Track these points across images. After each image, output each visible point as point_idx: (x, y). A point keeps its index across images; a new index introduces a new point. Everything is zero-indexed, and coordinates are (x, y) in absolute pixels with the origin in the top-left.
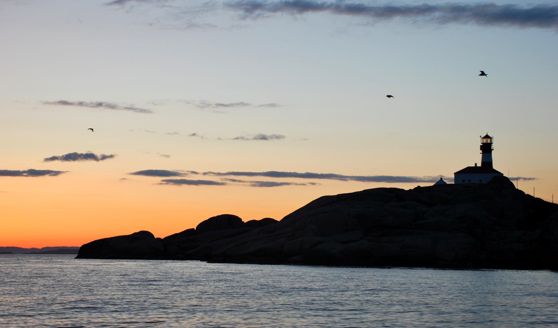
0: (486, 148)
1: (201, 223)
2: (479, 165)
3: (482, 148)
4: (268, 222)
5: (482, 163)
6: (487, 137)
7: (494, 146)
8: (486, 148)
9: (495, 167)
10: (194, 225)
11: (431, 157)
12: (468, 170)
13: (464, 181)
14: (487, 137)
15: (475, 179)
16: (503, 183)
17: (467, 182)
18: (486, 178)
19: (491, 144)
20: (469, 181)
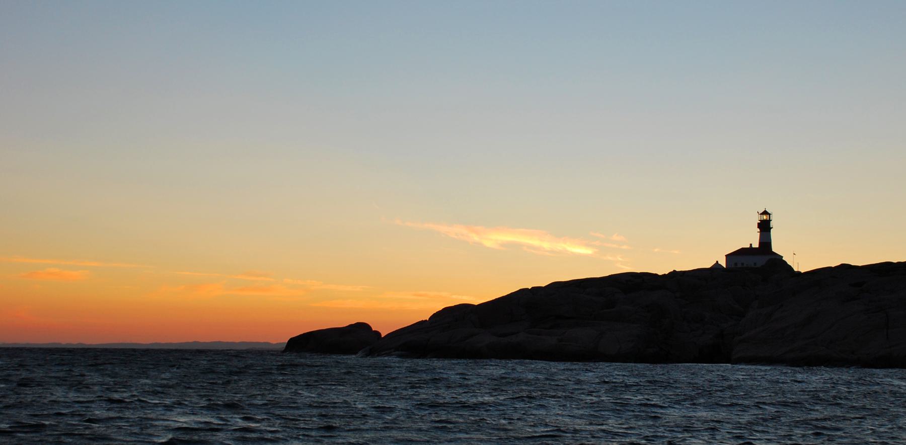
0: (765, 227)
1: (523, 291)
2: (756, 245)
3: (759, 226)
4: (656, 275)
5: (760, 243)
6: (765, 213)
7: (772, 224)
8: (765, 227)
9: (775, 249)
10: (543, 284)
11: (691, 240)
12: (742, 252)
13: (736, 264)
14: (765, 213)
15: (749, 261)
16: (778, 262)
17: (739, 266)
18: (761, 261)
19: (770, 220)
20: (743, 264)
